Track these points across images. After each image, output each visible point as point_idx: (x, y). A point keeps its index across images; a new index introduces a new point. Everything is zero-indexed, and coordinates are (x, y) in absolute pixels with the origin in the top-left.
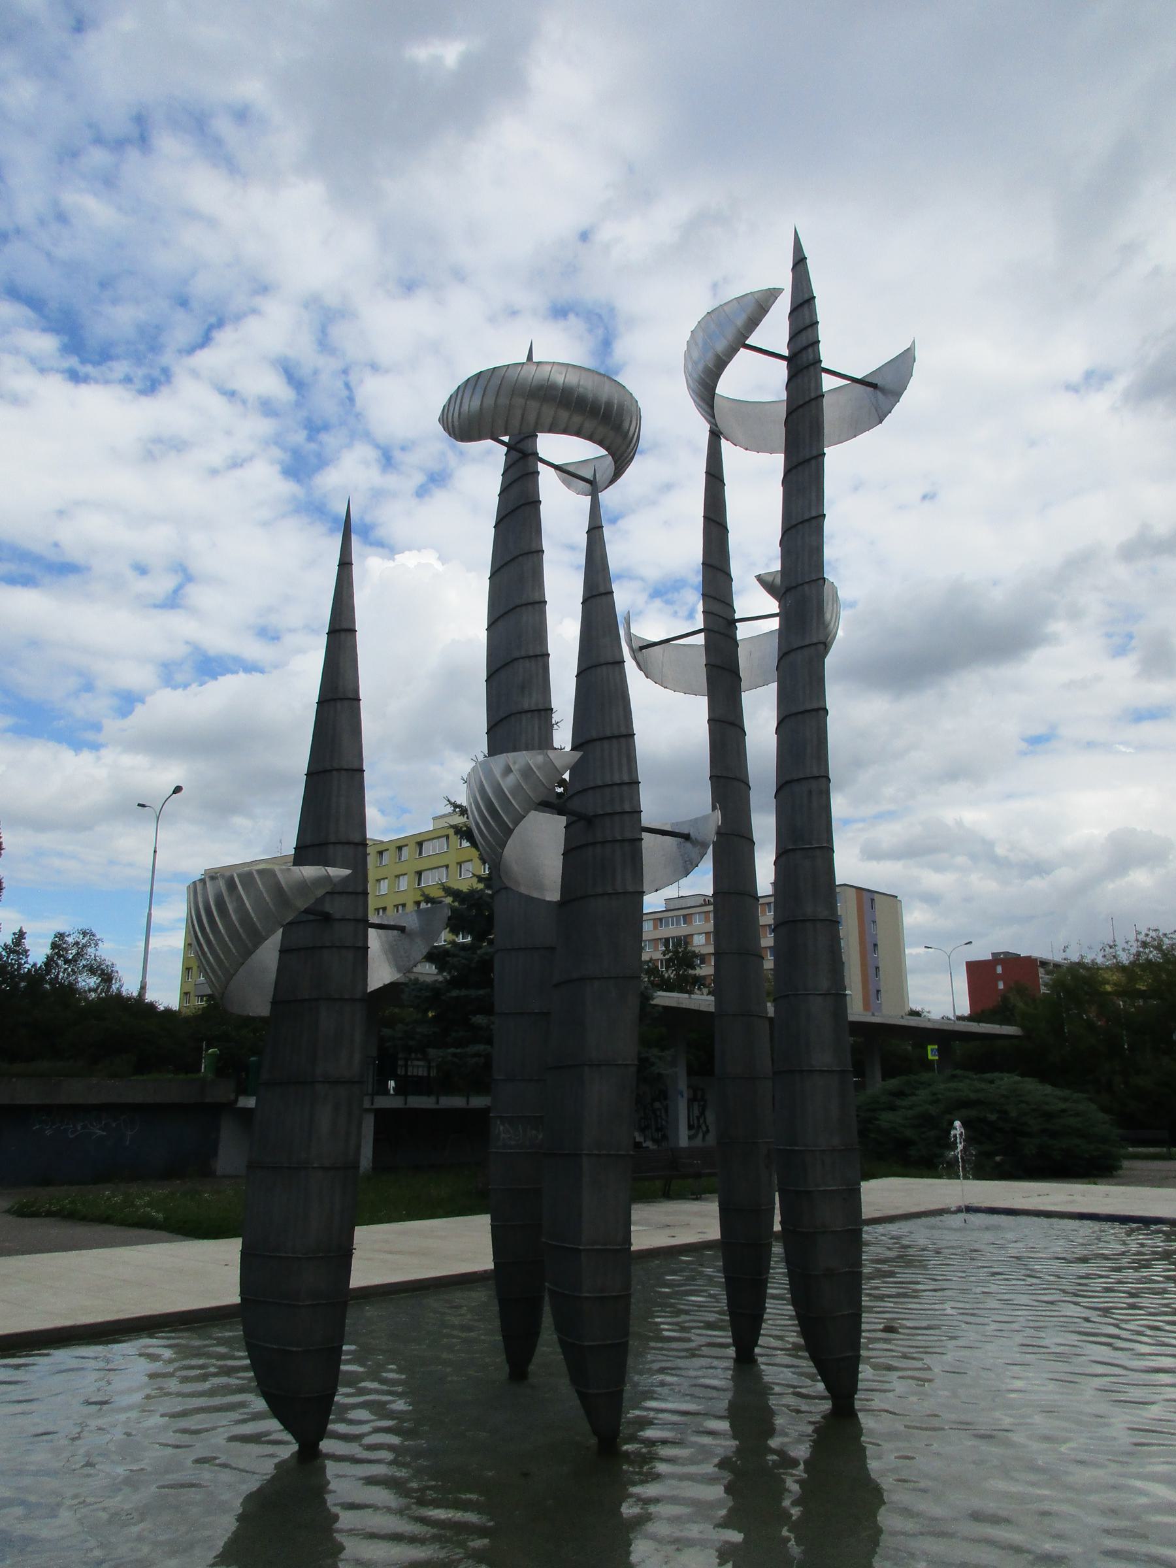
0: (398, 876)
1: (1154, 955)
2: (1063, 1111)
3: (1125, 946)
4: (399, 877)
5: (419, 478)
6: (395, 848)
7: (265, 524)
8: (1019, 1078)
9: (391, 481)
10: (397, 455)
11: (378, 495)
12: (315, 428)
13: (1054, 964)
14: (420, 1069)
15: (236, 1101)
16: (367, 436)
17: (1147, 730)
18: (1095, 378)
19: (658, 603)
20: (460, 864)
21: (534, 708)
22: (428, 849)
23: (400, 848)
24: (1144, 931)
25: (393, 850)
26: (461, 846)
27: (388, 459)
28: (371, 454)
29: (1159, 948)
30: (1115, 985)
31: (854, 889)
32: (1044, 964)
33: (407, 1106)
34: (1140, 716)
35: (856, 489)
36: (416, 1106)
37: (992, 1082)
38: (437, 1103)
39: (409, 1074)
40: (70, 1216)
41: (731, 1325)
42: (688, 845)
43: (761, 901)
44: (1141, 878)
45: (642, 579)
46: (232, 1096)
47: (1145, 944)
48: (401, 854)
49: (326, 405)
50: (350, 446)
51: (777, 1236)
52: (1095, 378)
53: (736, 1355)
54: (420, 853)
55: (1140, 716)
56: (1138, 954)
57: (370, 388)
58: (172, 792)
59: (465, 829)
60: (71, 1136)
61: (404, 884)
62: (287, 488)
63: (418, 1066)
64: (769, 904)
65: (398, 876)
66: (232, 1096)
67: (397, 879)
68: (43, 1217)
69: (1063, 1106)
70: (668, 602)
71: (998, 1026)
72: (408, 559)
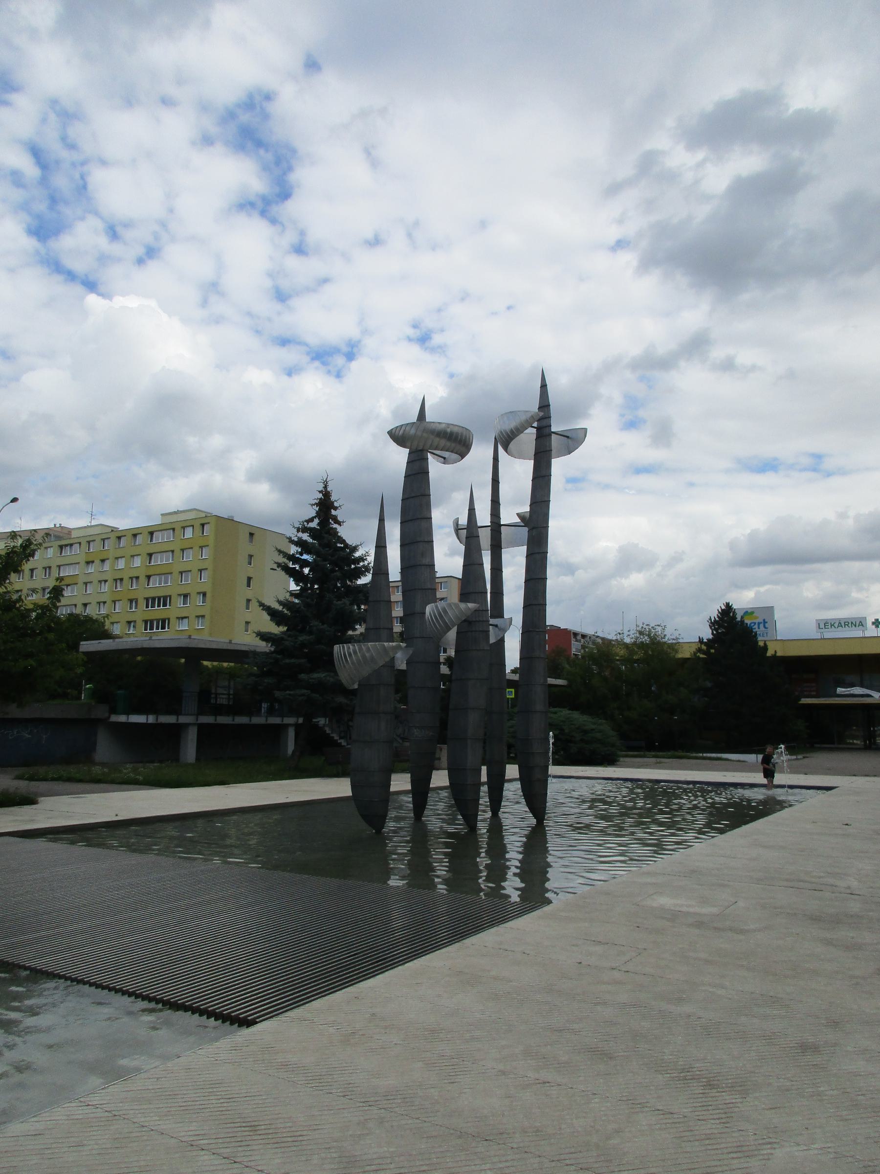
0: (133, 556)
1: (646, 639)
2: (593, 730)
3: (628, 633)
4: (133, 557)
5: (141, 251)
6: (131, 535)
7: (12, 271)
8: (568, 712)
9: (116, 249)
10: (119, 229)
11: (104, 259)
12: (54, 200)
13: (582, 635)
14: (224, 700)
15: (109, 717)
16: (97, 213)
17: (644, 480)
18: (620, 245)
19: (317, 364)
20: (183, 550)
21: (427, 564)
22: (159, 537)
23: (135, 536)
24: (641, 625)
25: (129, 537)
26: (184, 537)
27: (113, 233)
28: (99, 224)
29: (649, 635)
30: (622, 656)
31: (457, 580)
32: (575, 634)
33: (251, 723)
34: (640, 470)
35: (463, 299)
36: (222, 722)
37: (555, 713)
38: (233, 720)
39: (218, 703)
40: (70, 780)
41: (524, 795)
42: (497, 629)
43: (391, 585)
44: (636, 580)
45: (306, 345)
46: (107, 715)
47: (641, 633)
48: (136, 540)
49: (61, 182)
50: (82, 219)
51: (484, 784)
52: (620, 245)
53: (778, 656)
54: (151, 540)
55: (640, 470)
56: (637, 638)
57: (98, 177)
58: (10, 502)
59: (283, 564)
60: (10, 738)
61: (137, 562)
62: (30, 243)
63: (223, 698)
64: (398, 587)
65: (133, 556)
66: (107, 715)
67: (132, 559)
68: (49, 781)
69: (593, 727)
70: (324, 364)
71: (554, 680)
72: (119, 301)
